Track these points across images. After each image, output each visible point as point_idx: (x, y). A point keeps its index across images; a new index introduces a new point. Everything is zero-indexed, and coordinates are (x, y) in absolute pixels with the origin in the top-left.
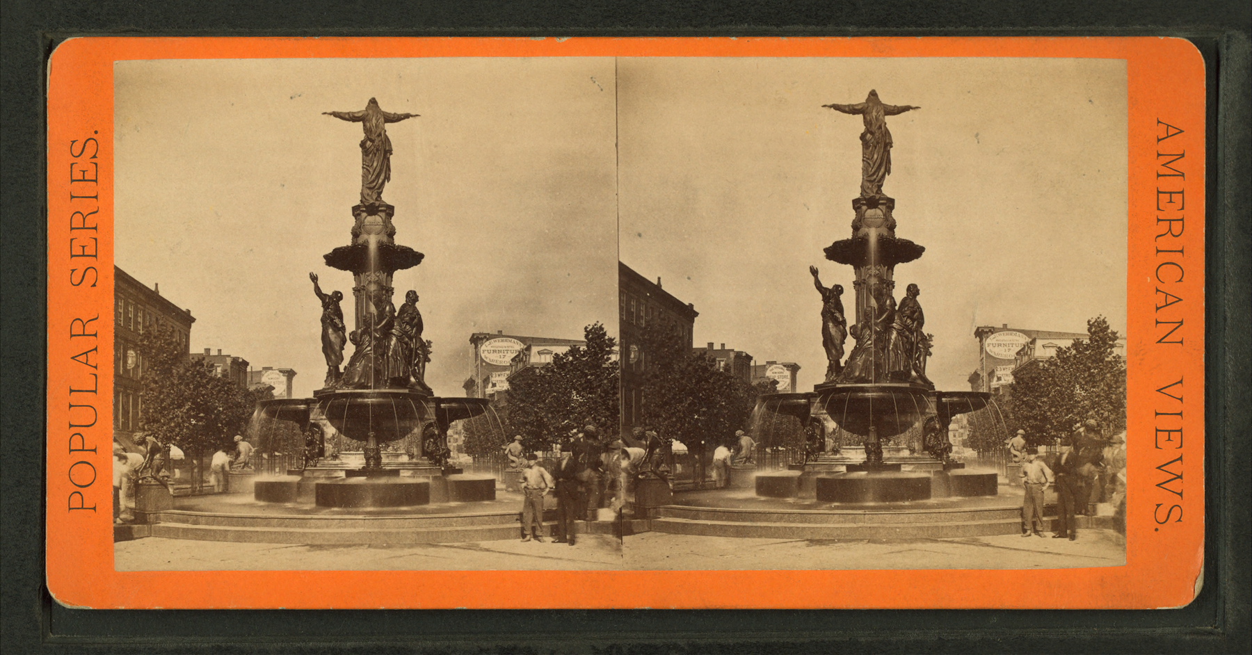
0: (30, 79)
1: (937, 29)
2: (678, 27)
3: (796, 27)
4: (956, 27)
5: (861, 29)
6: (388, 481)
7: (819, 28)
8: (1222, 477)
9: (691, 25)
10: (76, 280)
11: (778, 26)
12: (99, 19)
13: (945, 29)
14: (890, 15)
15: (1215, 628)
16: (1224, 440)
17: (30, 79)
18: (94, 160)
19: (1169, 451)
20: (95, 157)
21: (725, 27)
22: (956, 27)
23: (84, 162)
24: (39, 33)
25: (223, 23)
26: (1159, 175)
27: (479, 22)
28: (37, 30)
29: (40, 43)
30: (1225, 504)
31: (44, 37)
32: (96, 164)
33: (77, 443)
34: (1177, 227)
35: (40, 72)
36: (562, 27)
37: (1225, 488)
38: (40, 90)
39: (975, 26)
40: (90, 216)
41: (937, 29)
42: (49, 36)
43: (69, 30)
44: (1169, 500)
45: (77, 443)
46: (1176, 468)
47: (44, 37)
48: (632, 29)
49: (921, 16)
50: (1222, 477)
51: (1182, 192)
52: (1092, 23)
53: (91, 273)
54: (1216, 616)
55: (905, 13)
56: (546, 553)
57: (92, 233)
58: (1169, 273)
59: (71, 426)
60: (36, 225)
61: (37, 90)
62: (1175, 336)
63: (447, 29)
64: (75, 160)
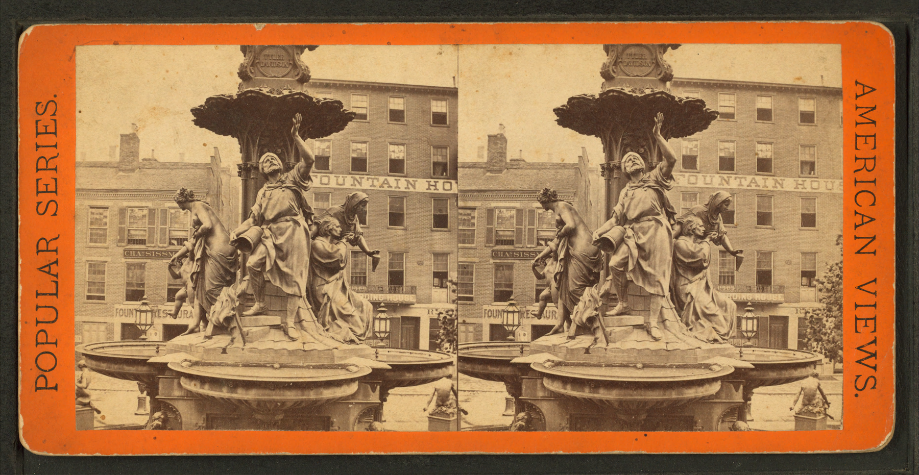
0: (6, 57)
1: (695, 16)
2: (498, 15)
3: (588, 15)
4: (709, 15)
5: (637, 16)
6: (438, 373)
7: (605, 16)
8: (912, 356)
9: (508, 14)
10: (41, 210)
11: (573, 14)
12: (58, 11)
13: (701, 16)
14: (658, 6)
15: (907, 470)
16: (913, 328)
17: (6, 57)
18: (54, 117)
19: (865, 335)
20: (54, 114)
21: (534, 16)
22: (709, 15)
23: (46, 119)
24: (13, 21)
25: (153, 13)
26: (857, 124)
27: (347, 12)
28: (11, 19)
29: (13, 28)
30: (914, 377)
31: (17, 24)
32: (55, 121)
33: (42, 338)
34: (870, 165)
35: (14, 51)
36: (410, 16)
37: (914, 364)
38: (14, 65)
39: (723, 14)
40: (51, 160)
41: (695, 16)
42: (21, 24)
43: (36, 19)
44: (866, 372)
45: (42, 338)
46: (871, 348)
47: (17, 24)
48: (463, 17)
49: (682, 6)
50: (912, 356)
51: (874, 136)
52: (812, 12)
53: (53, 205)
54: (907, 462)
55: (670, 4)
56: (646, 435)
57: (52, 174)
58: (865, 199)
59: (38, 322)
60: (11, 167)
61: (11, 65)
62: (870, 248)
63: (323, 18)
64: (40, 117)
